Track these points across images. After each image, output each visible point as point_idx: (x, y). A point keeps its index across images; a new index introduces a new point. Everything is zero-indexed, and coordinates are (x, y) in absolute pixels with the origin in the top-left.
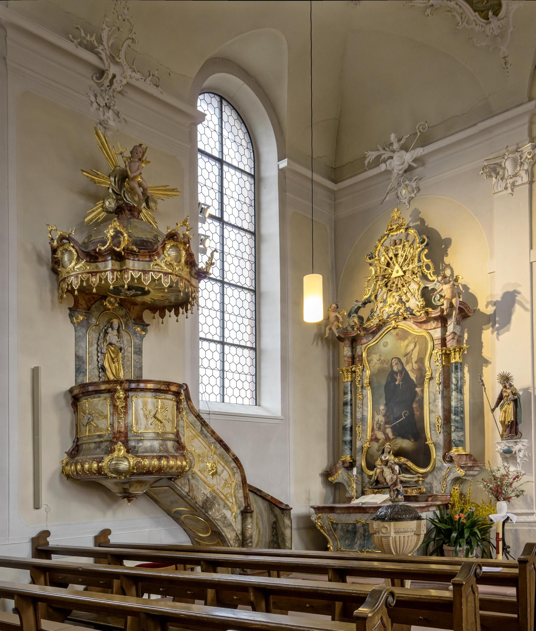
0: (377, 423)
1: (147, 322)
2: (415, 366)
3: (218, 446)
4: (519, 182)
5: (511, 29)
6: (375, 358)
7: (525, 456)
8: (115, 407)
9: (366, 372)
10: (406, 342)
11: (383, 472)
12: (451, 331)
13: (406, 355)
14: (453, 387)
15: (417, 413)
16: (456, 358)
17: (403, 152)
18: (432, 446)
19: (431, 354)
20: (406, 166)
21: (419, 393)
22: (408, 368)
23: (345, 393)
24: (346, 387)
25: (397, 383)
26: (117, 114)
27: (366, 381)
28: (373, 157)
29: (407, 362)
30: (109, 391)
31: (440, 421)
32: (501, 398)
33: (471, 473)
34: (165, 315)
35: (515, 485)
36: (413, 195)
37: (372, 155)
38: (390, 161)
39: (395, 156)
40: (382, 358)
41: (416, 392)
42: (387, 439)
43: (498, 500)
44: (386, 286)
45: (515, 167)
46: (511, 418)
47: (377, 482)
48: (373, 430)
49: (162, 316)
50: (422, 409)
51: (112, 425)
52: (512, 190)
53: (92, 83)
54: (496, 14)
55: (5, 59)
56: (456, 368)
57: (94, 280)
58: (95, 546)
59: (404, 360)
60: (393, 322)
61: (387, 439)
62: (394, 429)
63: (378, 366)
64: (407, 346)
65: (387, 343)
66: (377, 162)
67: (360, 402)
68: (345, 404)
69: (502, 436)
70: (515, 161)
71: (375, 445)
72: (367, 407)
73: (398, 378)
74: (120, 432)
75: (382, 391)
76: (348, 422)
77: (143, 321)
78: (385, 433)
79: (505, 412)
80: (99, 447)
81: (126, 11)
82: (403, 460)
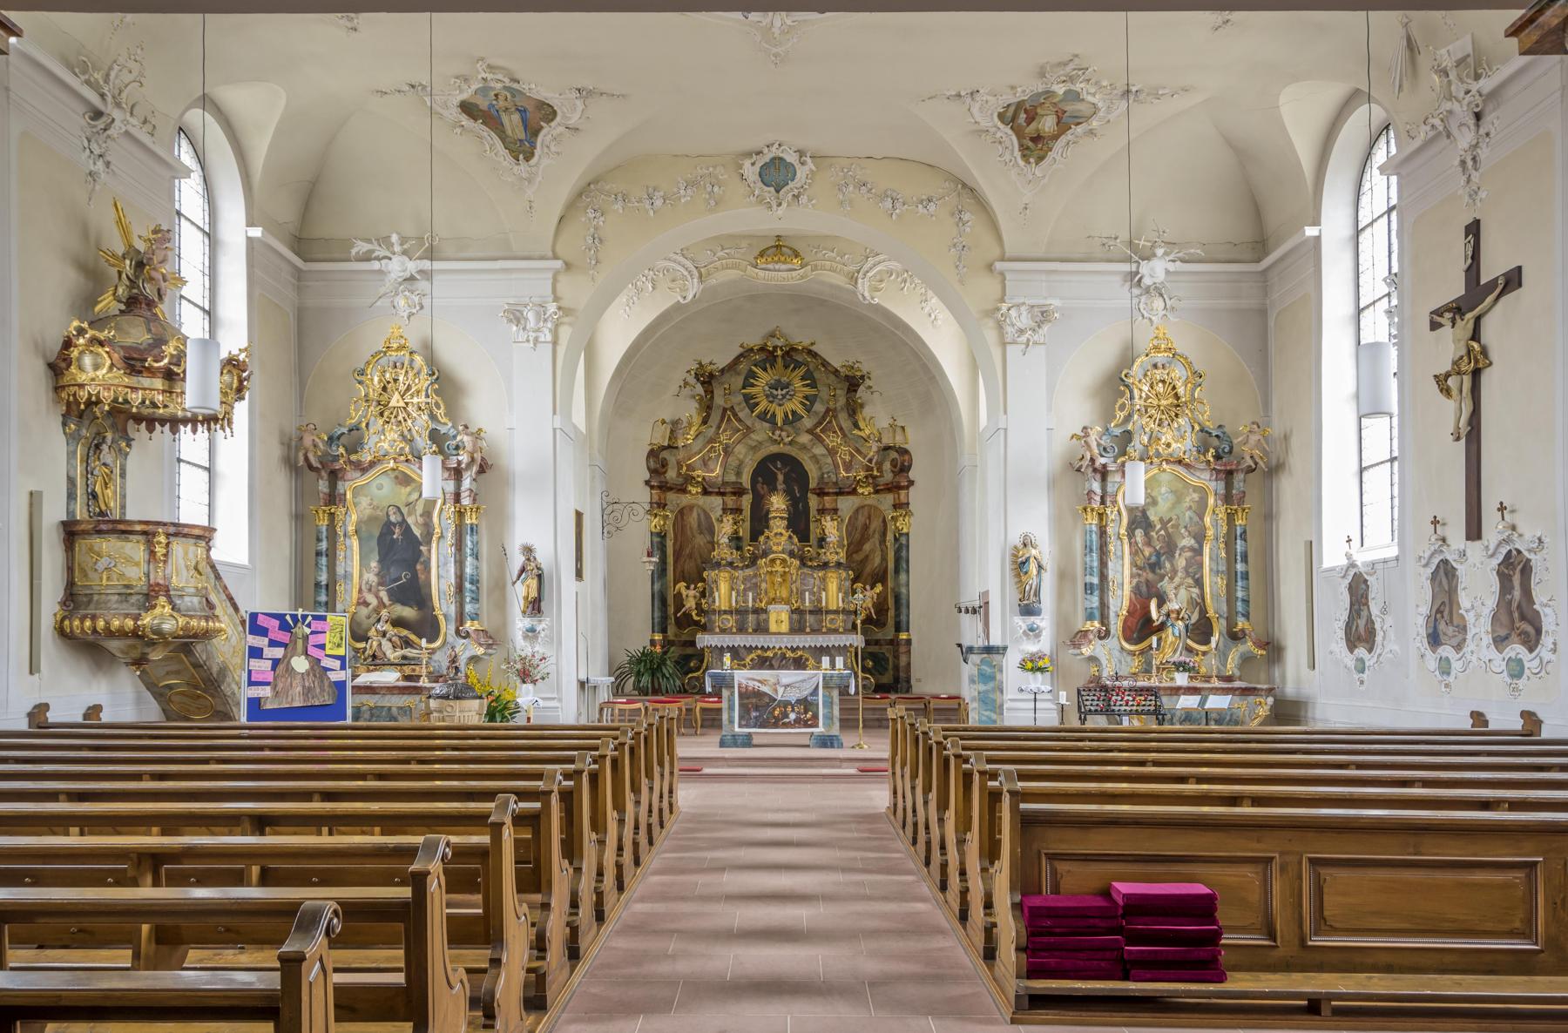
0: (367, 583)
1: (132, 436)
2: (420, 520)
3: (229, 604)
4: (542, 339)
5: (540, 179)
6: (364, 501)
7: (546, 636)
8: (152, 553)
9: (351, 517)
10: (408, 489)
11: (380, 645)
12: (468, 486)
13: (408, 505)
14: (468, 551)
15: (422, 577)
16: (469, 520)
17: (405, 258)
18: (441, 618)
19: (441, 510)
20: (407, 275)
21: (425, 553)
22: (410, 521)
23: (319, 540)
24: (319, 532)
25: (395, 537)
26: (108, 164)
27: (351, 528)
28: (364, 250)
29: (410, 514)
30: (144, 533)
31: (452, 589)
32: (523, 570)
33: (490, 651)
34: (154, 429)
35: (542, 666)
36: (414, 311)
37: (361, 247)
38: (386, 261)
39: (395, 259)
40: (375, 503)
41: (421, 551)
42: (382, 605)
43: (524, 682)
44: (382, 414)
45: (538, 321)
46: (534, 594)
47: (374, 657)
48: (360, 591)
49: (151, 429)
50: (429, 572)
51: (148, 575)
52: (535, 344)
53: (83, 122)
54: (527, 159)
55: (7, 89)
56: (472, 529)
57: (134, 396)
58: (30, 727)
59: (405, 510)
60: (392, 461)
61: (382, 605)
62: (391, 593)
63: (368, 512)
64: (410, 494)
65: (382, 485)
66: (367, 258)
67: (342, 554)
68: (318, 554)
69: (524, 612)
70: (538, 314)
71: (364, 611)
72: (352, 561)
73: (397, 530)
74: (158, 584)
75: (374, 543)
76: (323, 578)
77: (127, 434)
78: (377, 597)
79: (528, 586)
80: (127, 601)
81: (139, 51)
82: (405, 632)
